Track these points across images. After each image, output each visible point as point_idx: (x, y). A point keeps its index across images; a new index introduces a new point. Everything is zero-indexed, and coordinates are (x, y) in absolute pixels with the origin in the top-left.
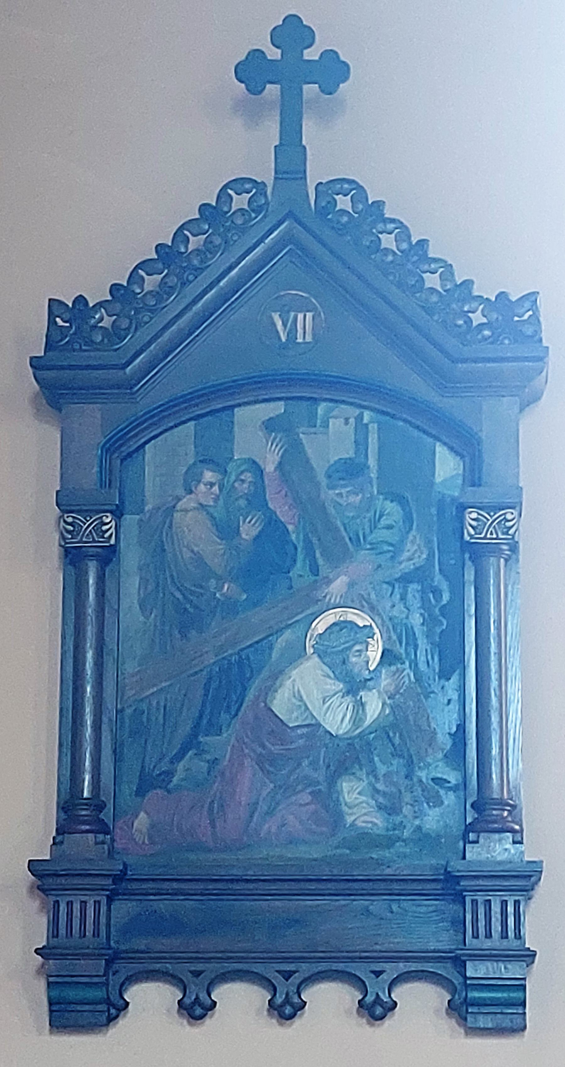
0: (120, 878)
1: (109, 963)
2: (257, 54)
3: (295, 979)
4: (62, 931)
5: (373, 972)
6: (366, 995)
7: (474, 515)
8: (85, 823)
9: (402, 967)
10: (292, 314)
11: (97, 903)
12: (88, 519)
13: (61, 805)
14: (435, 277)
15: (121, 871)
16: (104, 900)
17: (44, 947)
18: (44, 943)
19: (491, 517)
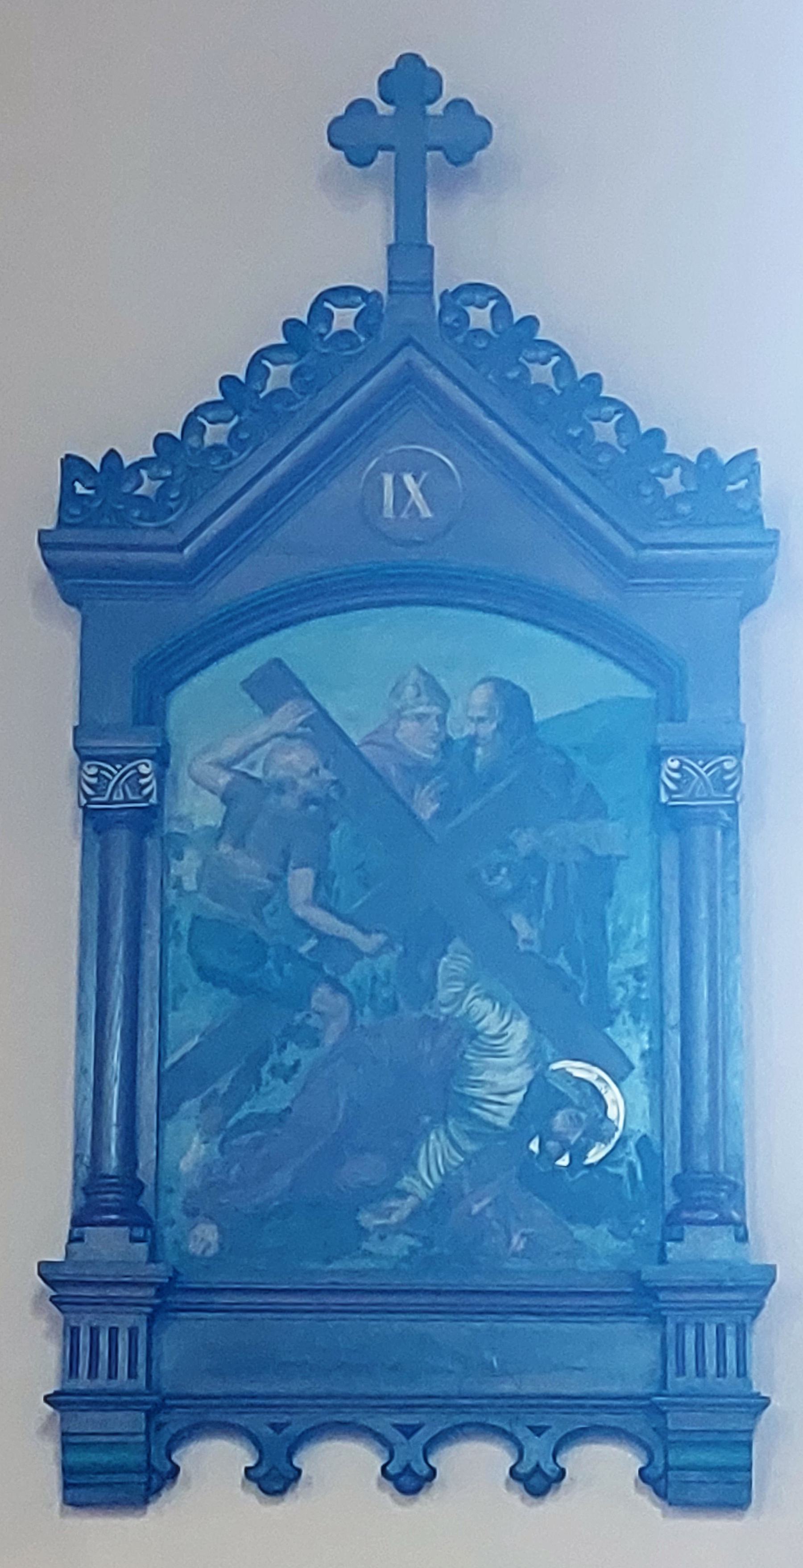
0: (161, 1290)
1: (148, 1419)
3: (421, 1437)
5: (531, 1428)
13: (81, 1184)
15: (170, 1278)
17: (56, 1393)
19: (119, 771)
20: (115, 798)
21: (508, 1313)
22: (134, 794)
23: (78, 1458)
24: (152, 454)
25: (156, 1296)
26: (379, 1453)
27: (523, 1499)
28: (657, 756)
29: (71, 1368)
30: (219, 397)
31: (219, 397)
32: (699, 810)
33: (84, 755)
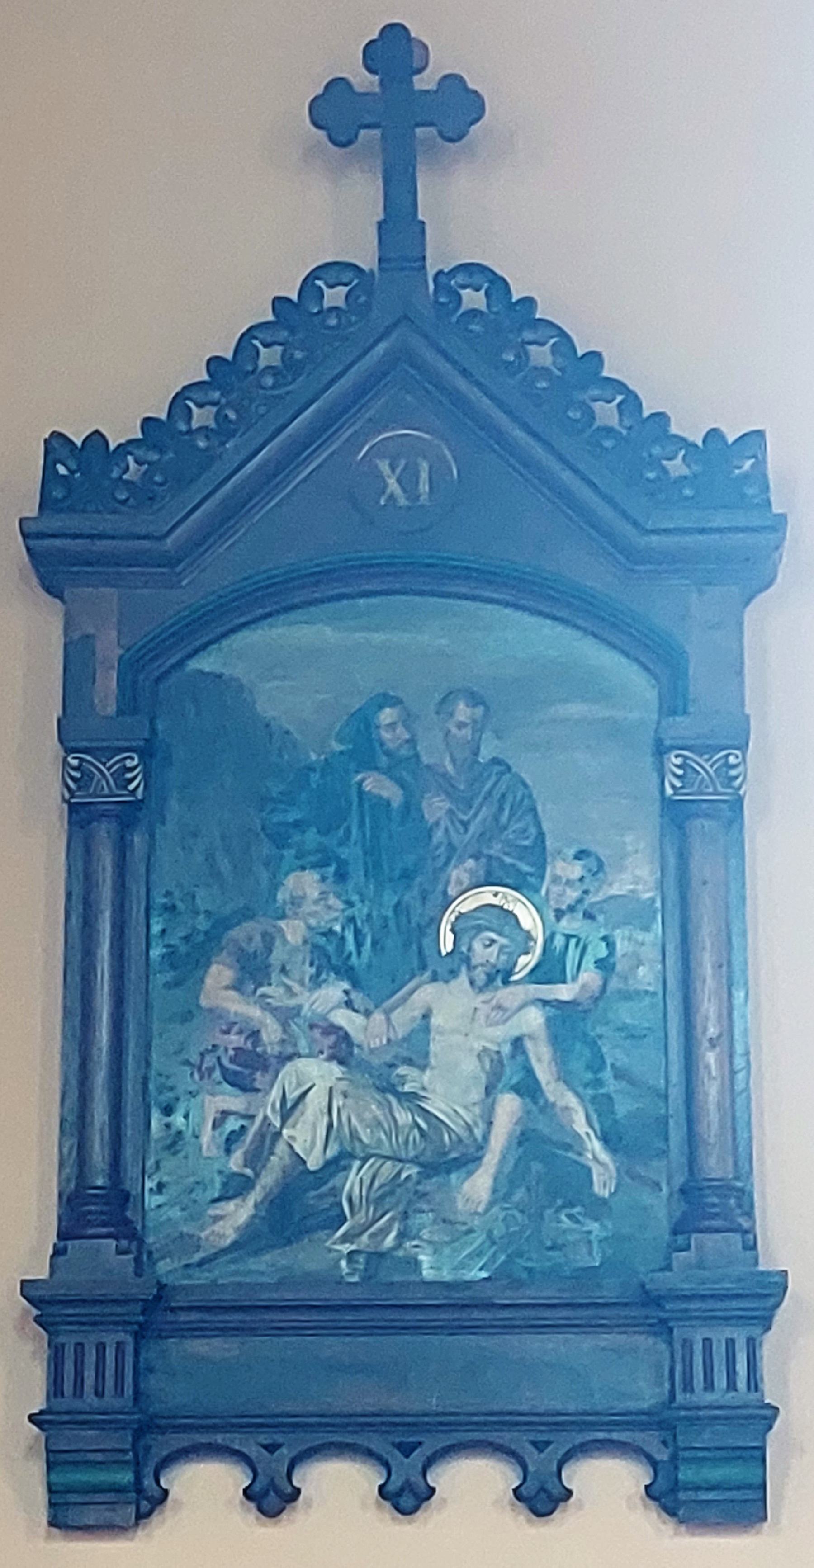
1: (138, 1434)
2: (337, 85)
4: (68, 1387)
7: (678, 761)
14: (610, 409)
16: (129, 1339)
17: (41, 1412)
18: (43, 1407)
21: (509, 1328)
22: (723, 787)
23: (62, 1478)
27: (529, 1521)
28: (660, 750)
29: (55, 1387)
30: (206, 377)
31: (206, 377)
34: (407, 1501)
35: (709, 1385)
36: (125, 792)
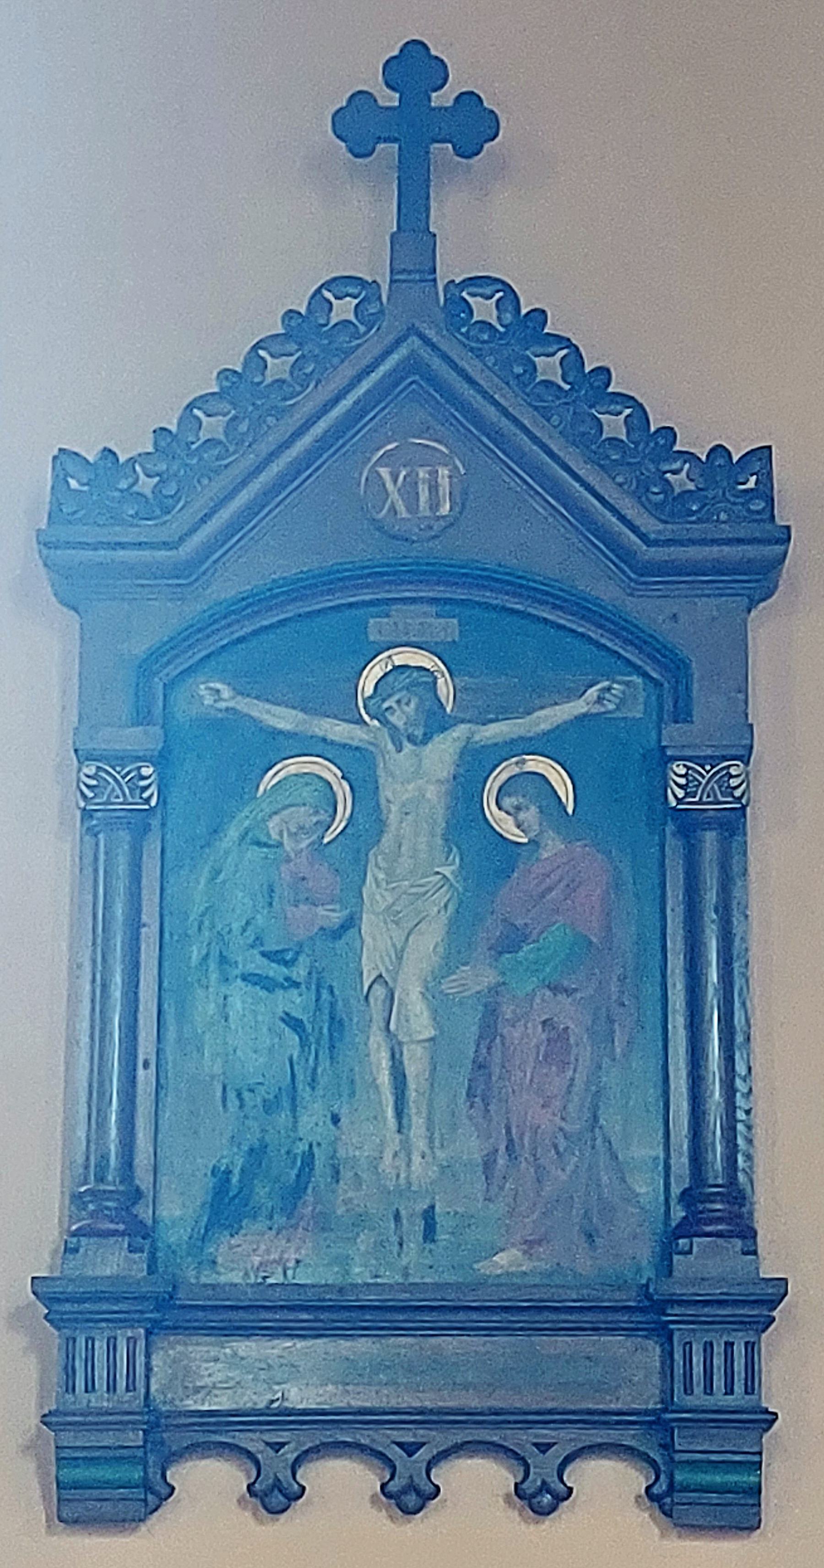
3: (423, 1455)
6: (392, 1477)
7: (683, 771)
8: (719, 1220)
9: (459, 1437)
10: (445, 509)
11: (132, 1341)
12: (708, 768)
19: (708, 772)
20: (705, 799)
22: (723, 796)
24: (150, 449)
25: (157, 1309)
26: (510, 1469)
32: (711, 813)
33: (83, 756)
34: (277, 1499)
35: (709, 1389)
36: (730, 799)
